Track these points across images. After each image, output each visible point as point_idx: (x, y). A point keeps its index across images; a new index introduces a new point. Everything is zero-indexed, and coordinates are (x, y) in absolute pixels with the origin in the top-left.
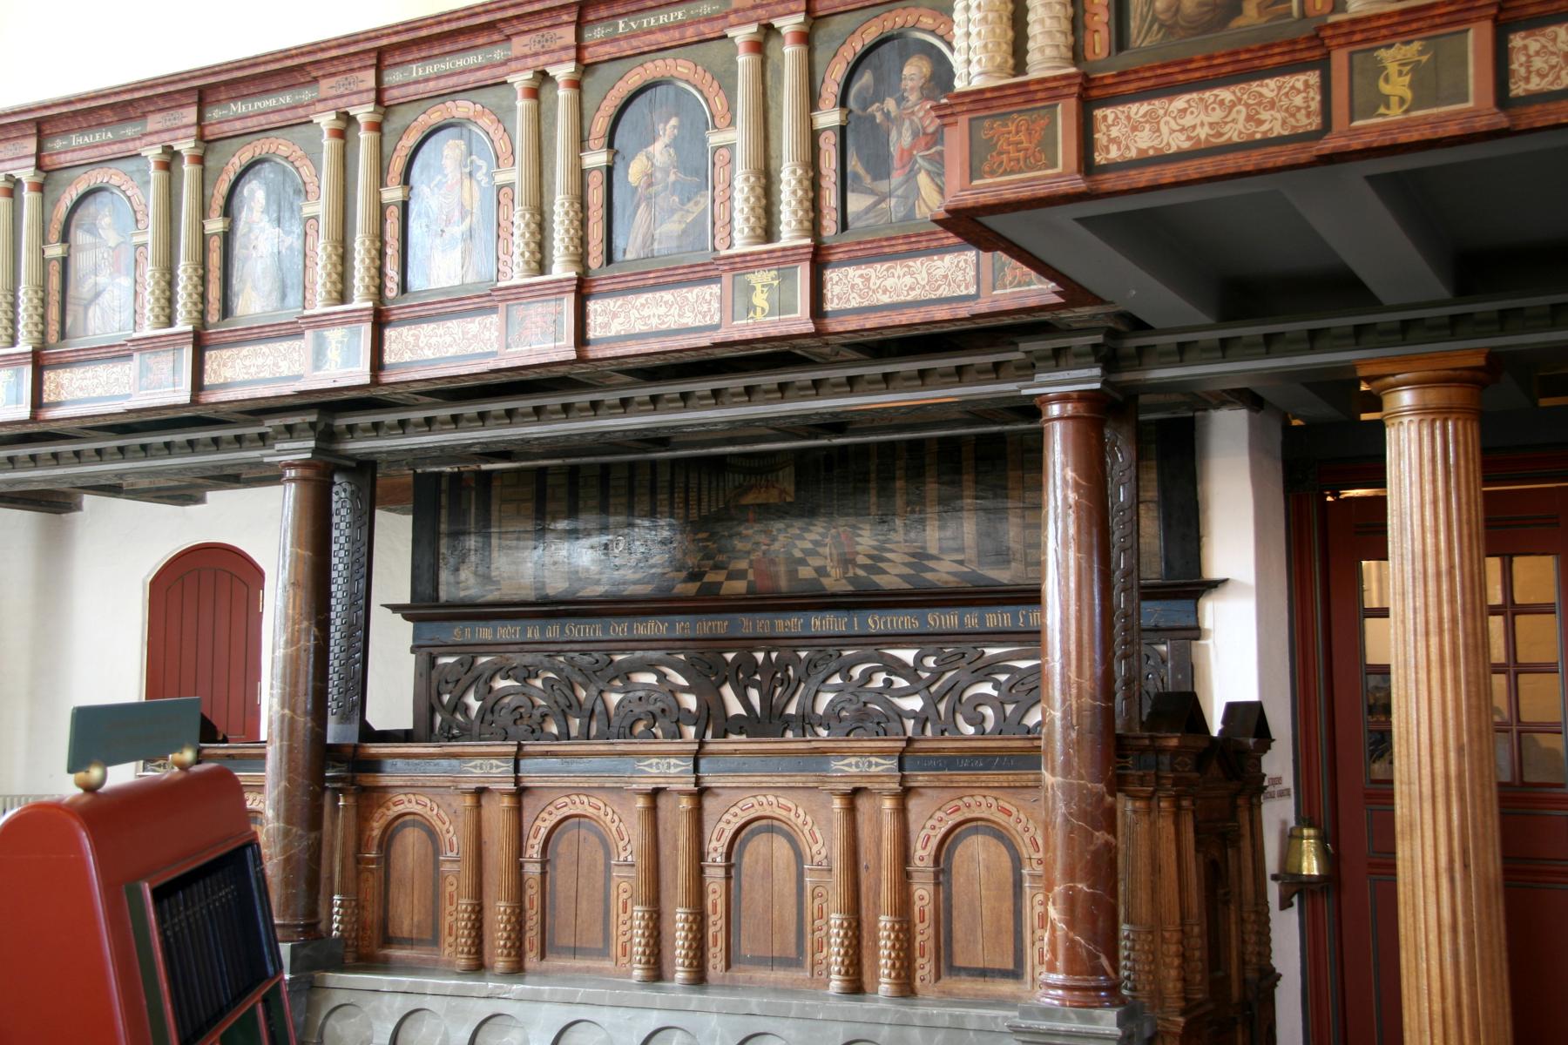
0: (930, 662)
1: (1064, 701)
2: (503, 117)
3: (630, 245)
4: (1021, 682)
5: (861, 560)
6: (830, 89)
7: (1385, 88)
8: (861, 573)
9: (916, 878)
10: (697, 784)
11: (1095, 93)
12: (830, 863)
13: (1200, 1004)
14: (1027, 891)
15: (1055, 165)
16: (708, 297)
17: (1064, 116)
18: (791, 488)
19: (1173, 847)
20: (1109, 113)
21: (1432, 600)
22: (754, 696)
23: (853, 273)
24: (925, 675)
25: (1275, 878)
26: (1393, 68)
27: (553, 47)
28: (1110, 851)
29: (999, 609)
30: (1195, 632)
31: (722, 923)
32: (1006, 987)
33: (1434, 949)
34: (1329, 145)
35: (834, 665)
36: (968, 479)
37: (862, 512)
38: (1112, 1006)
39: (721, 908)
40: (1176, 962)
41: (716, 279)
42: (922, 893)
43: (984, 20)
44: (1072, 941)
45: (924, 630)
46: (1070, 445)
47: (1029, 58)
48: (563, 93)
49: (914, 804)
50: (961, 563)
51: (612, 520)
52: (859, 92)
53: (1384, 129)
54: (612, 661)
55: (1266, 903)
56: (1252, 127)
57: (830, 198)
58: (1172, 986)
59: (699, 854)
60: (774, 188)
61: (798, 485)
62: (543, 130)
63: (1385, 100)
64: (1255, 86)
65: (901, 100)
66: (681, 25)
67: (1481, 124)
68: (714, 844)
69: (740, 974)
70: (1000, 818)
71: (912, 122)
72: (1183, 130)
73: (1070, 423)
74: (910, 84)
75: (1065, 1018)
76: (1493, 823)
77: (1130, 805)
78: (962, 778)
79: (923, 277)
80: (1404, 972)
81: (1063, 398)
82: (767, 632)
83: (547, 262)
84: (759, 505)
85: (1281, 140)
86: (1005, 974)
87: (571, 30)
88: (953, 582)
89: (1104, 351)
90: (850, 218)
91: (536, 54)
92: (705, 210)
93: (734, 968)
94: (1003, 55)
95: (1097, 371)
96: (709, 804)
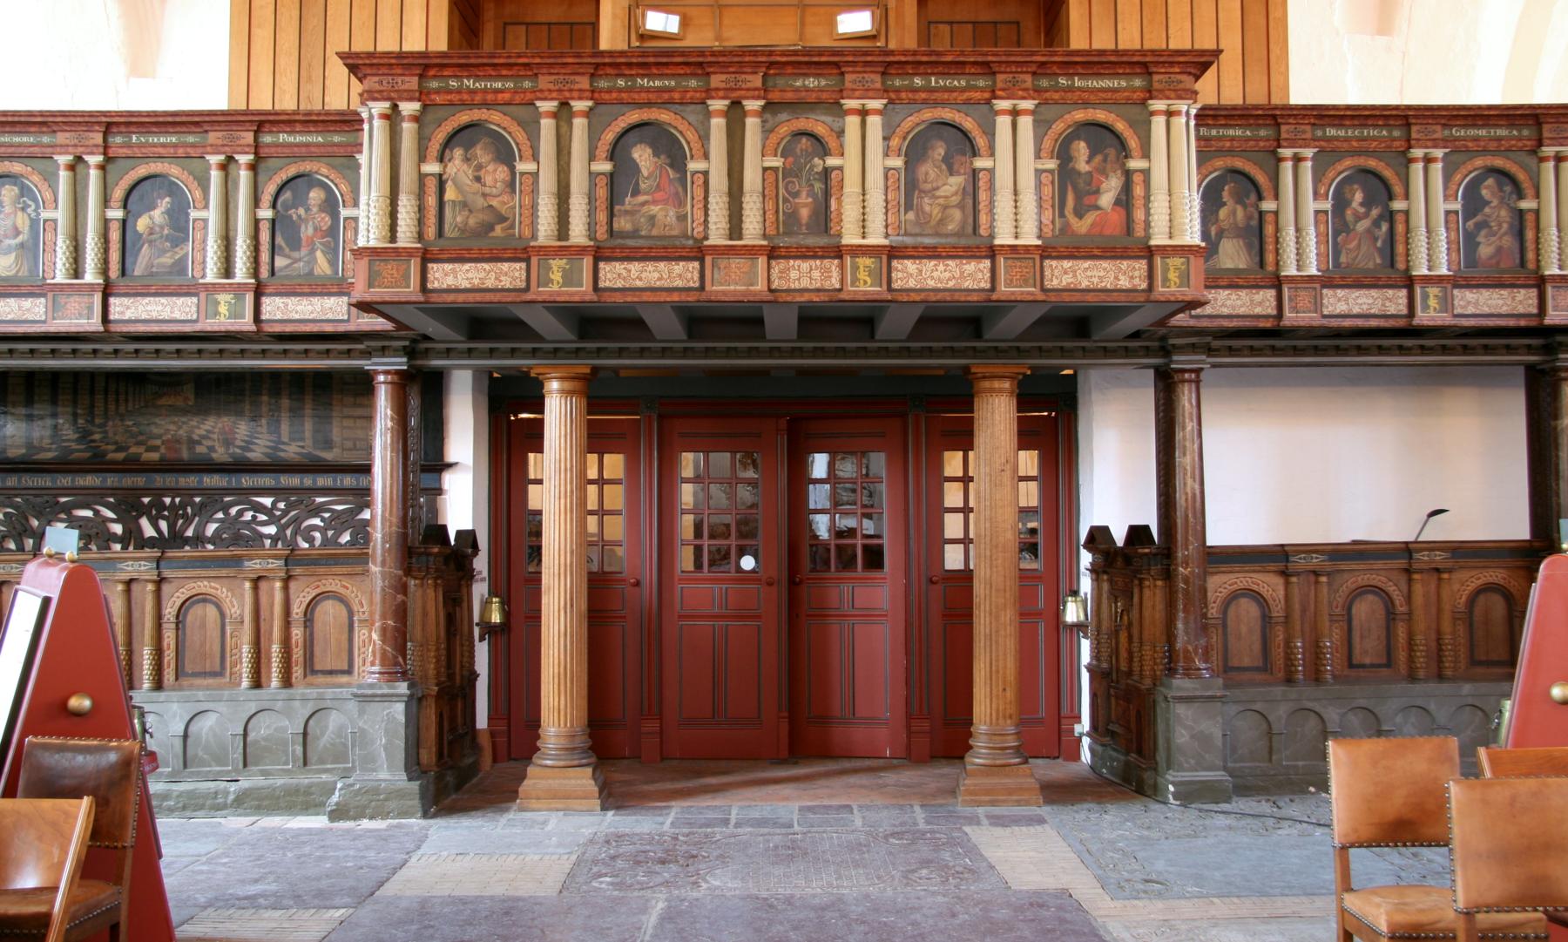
0: (282, 505)
1: (383, 529)
2: (51, 179)
3: (139, 268)
4: (338, 518)
5: (238, 443)
6: (266, 198)
7: (552, 276)
8: (238, 451)
9: (293, 625)
10: (158, 576)
11: (428, 256)
12: (242, 618)
13: (444, 682)
14: (356, 629)
15: (409, 287)
17: (414, 265)
18: (192, 397)
19: (434, 603)
21: (562, 482)
22: (163, 525)
23: (279, 301)
24: (278, 513)
25: (477, 624)
26: (555, 269)
27: (87, 143)
28: (404, 603)
29: (326, 475)
30: (439, 491)
31: (173, 655)
32: (344, 679)
33: (556, 645)
34: (529, 297)
35: (218, 506)
36: (308, 398)
37: (240, 414)
38: (404, 681)
39: (173, 646)
40: (434, 660)
41: (196, 295)
42: (297, 633)
43: (377, 214)
44: (385, 650)
45: (278, 486)
46: (389, 397)
47: (398, 235)
48: (94, 174)
49: (293, 585)
50: (303, 447)
51: (60, 409)
52: (284, 201)
53: (551, 294)
54: (58, 502)
55: (473, 637)
57: (265, 257)
58: (432, 672)
59: (159, 616)
60: (232, 247)
61: (197, 394)
62: (78, 190)
63: (552, 281)
65: (308, 210)
66: (175, 146)
68: (168, 610)
69: (185, 682)
70: (342, 591)
73: (389, 386)
74: (313, 202)
75: (380, 688)
76: (585, 586)
77: (413, 582)
78: (322, 570)
79: (318, 308)
80: (543, 656)
81: (386, 373)
82: (173, 485)
83: (80, 270)
84: (170, 406)
85: (508, 290)
86: (343, 672)
87: (101, 135)
88: (297, 458)
89: (408, 350)
90: (276, 269)
91: (75, 146)
92: (187, 254)
93: (180, 679)
94: (386, 232)
95: (405, 360)
96: (166, 588)
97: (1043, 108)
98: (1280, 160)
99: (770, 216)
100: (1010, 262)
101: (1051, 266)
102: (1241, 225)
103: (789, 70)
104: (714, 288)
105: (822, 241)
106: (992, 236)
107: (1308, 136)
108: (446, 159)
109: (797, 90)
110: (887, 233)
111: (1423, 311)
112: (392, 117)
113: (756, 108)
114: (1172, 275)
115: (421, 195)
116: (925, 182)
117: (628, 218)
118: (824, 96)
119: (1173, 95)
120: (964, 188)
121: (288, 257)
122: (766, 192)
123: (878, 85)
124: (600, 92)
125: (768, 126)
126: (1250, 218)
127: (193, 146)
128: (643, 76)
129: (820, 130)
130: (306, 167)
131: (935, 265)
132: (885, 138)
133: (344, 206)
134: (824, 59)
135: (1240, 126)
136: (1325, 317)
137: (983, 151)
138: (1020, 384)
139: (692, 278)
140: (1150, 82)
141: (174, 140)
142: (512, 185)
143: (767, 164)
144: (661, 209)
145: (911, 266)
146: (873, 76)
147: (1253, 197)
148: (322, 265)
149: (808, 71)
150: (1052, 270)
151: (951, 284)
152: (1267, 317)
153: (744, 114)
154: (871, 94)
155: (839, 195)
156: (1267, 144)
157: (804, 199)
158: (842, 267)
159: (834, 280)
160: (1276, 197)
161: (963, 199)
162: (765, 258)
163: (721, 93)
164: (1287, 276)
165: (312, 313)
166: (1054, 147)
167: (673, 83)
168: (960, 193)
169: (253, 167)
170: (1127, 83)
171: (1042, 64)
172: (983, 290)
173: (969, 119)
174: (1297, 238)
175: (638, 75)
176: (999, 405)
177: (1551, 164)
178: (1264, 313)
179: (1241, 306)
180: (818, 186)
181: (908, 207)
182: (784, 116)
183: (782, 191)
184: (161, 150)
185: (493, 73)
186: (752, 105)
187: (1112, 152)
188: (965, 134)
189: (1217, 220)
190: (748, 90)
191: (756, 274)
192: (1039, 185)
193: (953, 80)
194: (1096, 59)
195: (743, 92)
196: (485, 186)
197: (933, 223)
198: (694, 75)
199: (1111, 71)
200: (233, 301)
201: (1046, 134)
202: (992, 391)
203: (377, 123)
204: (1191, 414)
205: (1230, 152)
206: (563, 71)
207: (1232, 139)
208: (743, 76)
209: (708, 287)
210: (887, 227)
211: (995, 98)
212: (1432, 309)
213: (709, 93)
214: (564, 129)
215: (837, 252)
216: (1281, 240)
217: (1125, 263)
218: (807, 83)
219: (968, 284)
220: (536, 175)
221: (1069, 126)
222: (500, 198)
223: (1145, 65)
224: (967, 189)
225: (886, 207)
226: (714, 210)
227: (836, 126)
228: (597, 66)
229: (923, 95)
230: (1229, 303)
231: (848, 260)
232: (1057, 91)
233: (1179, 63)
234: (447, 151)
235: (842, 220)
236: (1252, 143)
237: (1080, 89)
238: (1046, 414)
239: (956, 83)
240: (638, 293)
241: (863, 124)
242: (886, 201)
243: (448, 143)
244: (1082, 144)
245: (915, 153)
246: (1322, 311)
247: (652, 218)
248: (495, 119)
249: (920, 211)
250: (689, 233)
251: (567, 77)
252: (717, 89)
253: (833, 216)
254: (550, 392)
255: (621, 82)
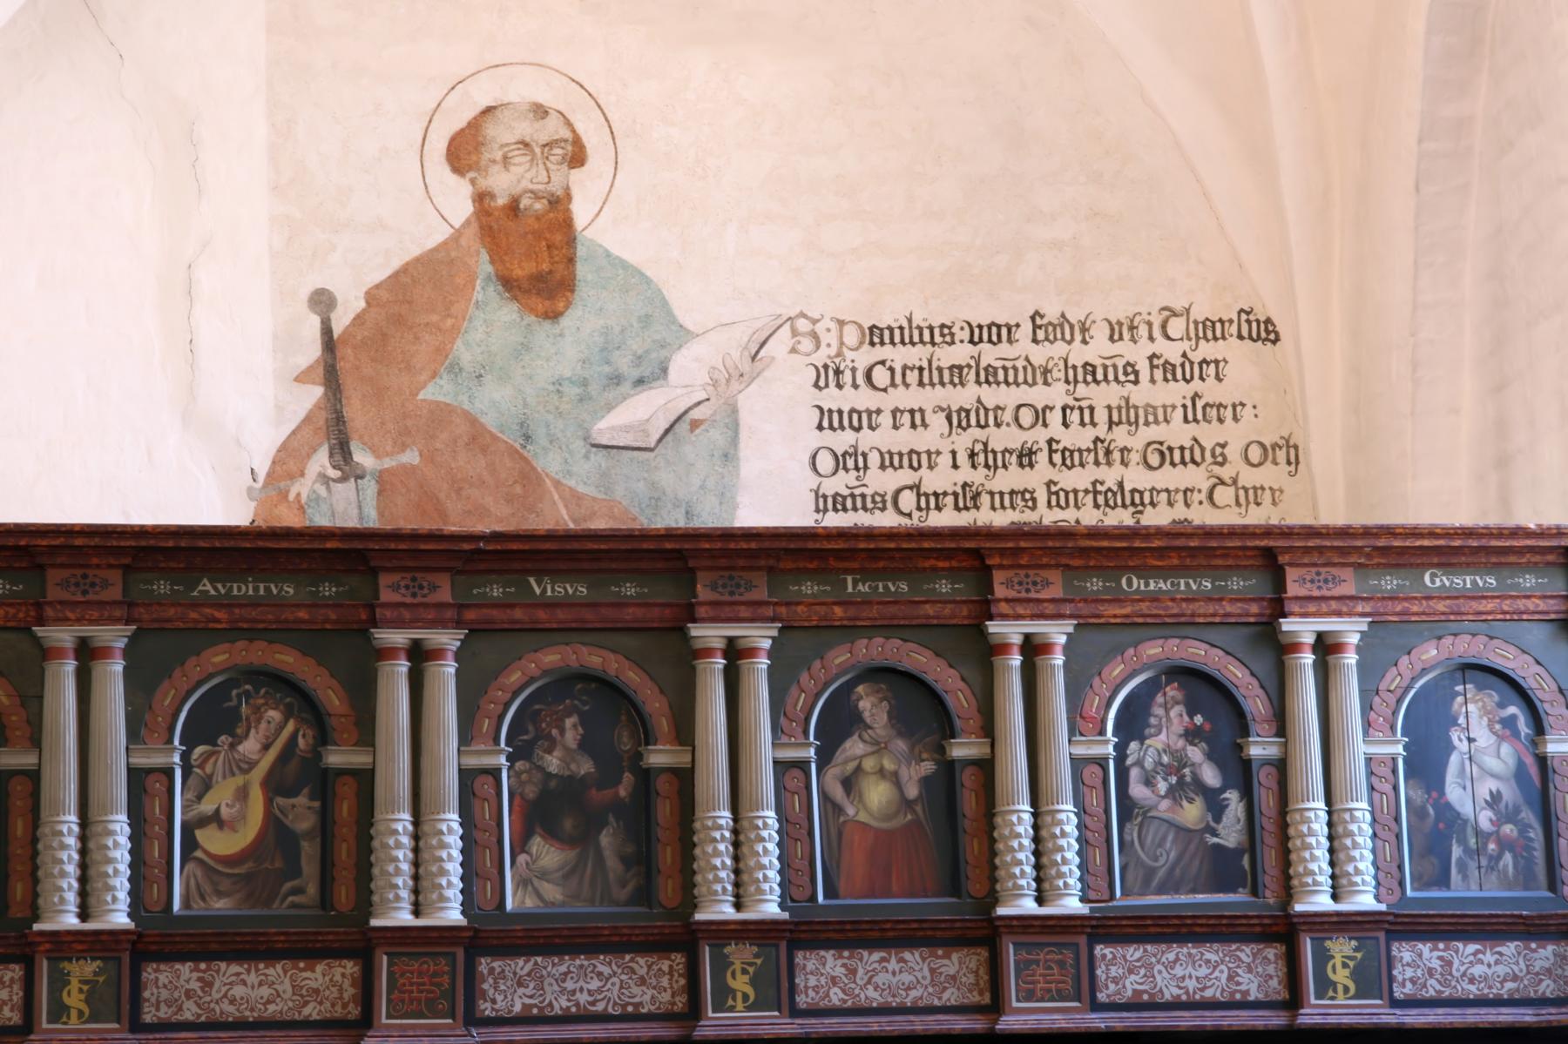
98: (47, 654)
111: (1319, 996)
131: (883, 960)
177: (402, 666)
212: (74, 1014)
246: (1391, 991)
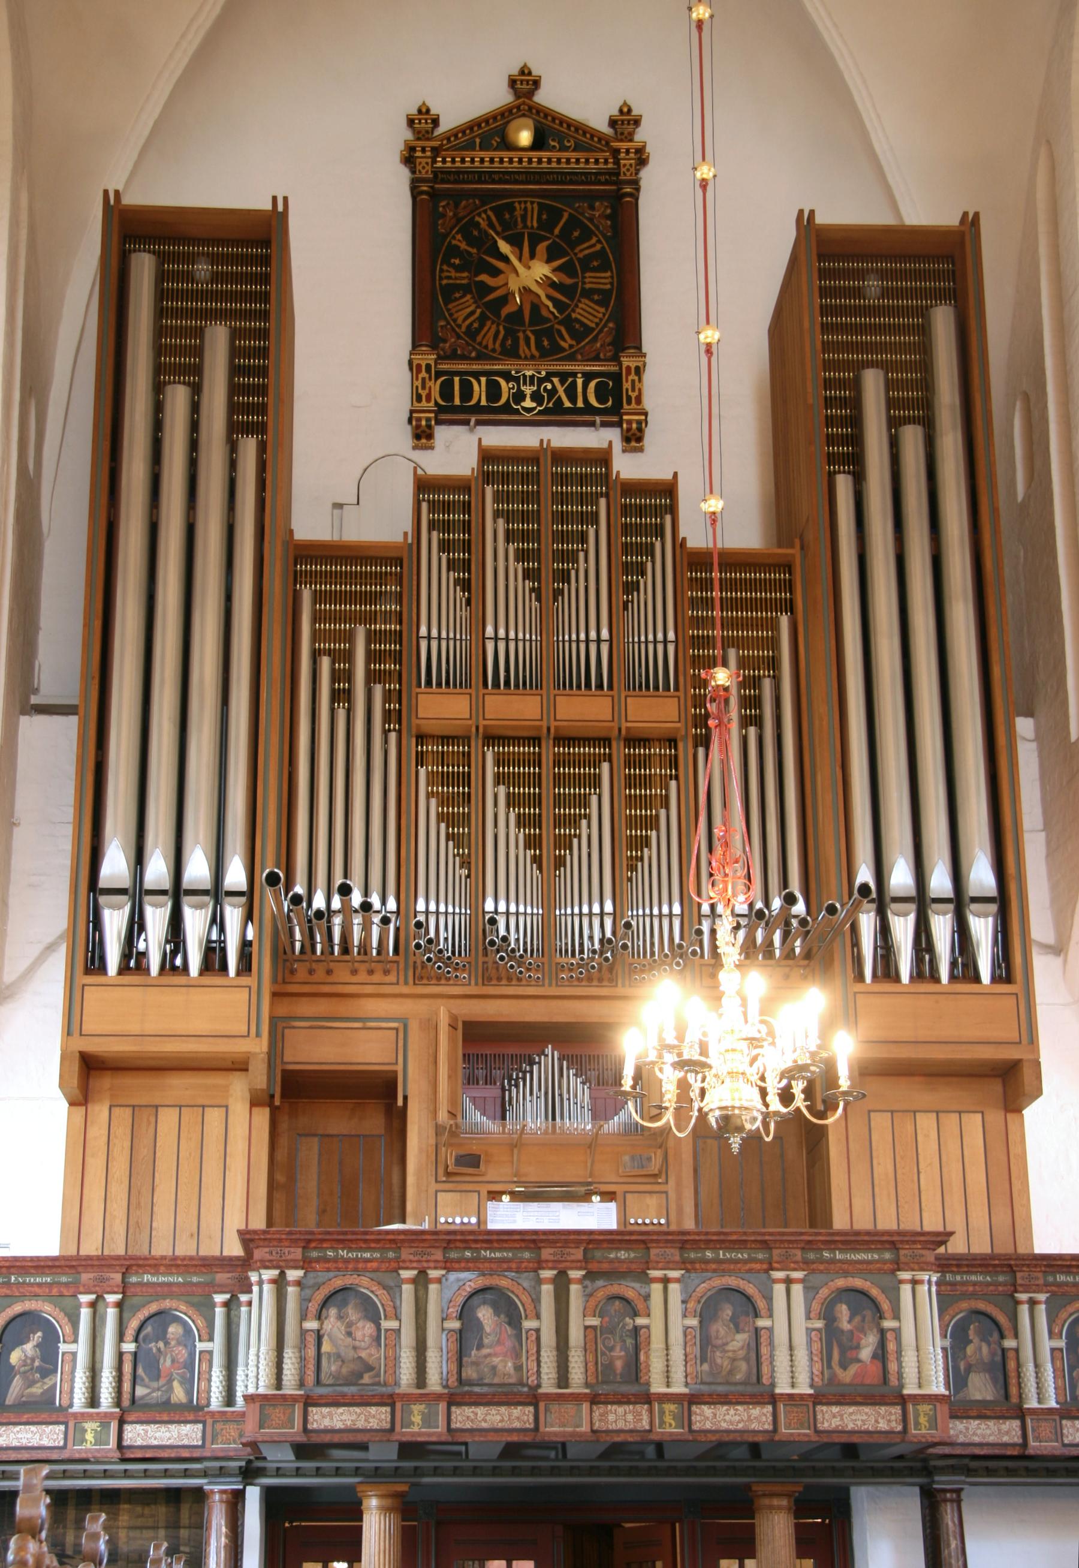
6: (130, 1333)
7: (413, 1419)
15: (294, 1428)
16: (57, 1431)
20: (314, 1409)
23: (139, 1428)
26: (416, 1412)
47: (284, 1383)
53: (413, 1434)
56: (366, 1424)
57: (127, 1386)
60: (97, 1378)
63: (413, 1423)
64: (368, 1408)
65: (166, 1343)
67: (443, 1439)
71: (172, 1355)
72: (341, 1421)
74: (172, 1336)
90: (136, 1398)
92: (55, 1384)
97: (811, 1278)
98: (1017, 1303)
99: (591, 1366)
100: (788, 1408)
101: (822, 1411)
102: (986, 1361)
103: (605, 1245)
104: (547, 1429)
105: (633, 1389)
106: (773, 1385)
107: (1041, 1282)
108: (323, 1317)
109: (611, 1261)
110: (686, 1382)
112: (280, 1283)
113: (578, 1276)
114: (923, 1420)
115: (302, 1345)
116: (717, 1338)
117: (474, 1368)
118: (634, 1266)
119: (916, 1267)
120: (749, 1344)
121: (147, 1387)
122: (587, 1347)
123: (677, 1258)
124: (452, 1262)
125: (588, 1291)
126: (993, 1354)
127: (67, 1284)
128: (485, 1249)
129: (630, 1294)
130: (167, 1304)
131: (727, 1410)
132: (683, 1302)
133: (200, 1340)
134: (633, 1238)
135: (981, 1273)
136: (1064, 1445)
137: (763, 1312)
138: (797, 1501)
139: (528, 1420)
140: (898, 1256)
141: (49, 1280)
142: (378, 1339)
143: (588, 1323)
144: (501, 1361)
145: (707, 1410)
146: (672, 1250)
147: (996, 1335)
148: (179, 1394)
149: (620, 1246)
150: (823, 1414)
151: (740, 1426)
152: (1014, 1445)
153: (569, 1281)
154: (671, 1265)
155: (647, 1350)
156: (1005, 1288)
157: (618, 1353)
158: (651, 1411)
159: (644, 1423)
160: (1016, 1336)
161: (748, 1353)
162: (588, 1404)
163: (550, 1265)
164: (1029, 1409)
165: (169, 1439)
166: (821, 1309)
167: (510, 1255)
168: (746, 1347)
169: (119, 1305)
170: (879, 1255)
171: (809, 1242)
172: (766, 1431)
173: (751, 1285)
174: (1037, 1373)
175: (482, 1248)
176: (779, 1522)
178: (1011, 1441)
179: (990, 1435)
180: (630, 1342)
181: (703, 1360)
182: (600, 1283)
183: (600, 1346)
184: (37, 1290)
185: (364, 1246)
186: (575, 1274)
187: (868, 1313)
188: (748, 1298)
189: (965, 1356)
190: (573, 1261)
191: (581, 1418)
192: (810, 1342)
193: (738, 1253)
194: (853, 1238)
195: (568, 1264)
196: (355, 1340)
197: (724, 1373)
198: (527, 1248)
199: (865, 1247)
200: (99, 1429)
201: (814, 1298)
202: (771, 1508)
203: (266, 1287)
204: (954, 1532)
205: (973, 1296)
206: (422, 1245)
207: (975, 1284)
208: (568, 1250)
209: (542, 1429)
210: (686, 1377)
211: (772, 1270)
213: (540, 1265)
214: (421, 1293)
215: (647, 1398)
216: (1022, 1375)
217: (883, 1408)
218: (619, 1255)
219: (754, 1426)
220: (398, 1331)
221: (833, 1292)
222: (368, 1351)
223: (893, 1243)
224: (751, 1344)
225: (686, 1361)
226: (546, 1363)
227: (643, 1292)
228: (449, 1241)
229: (714, 1266)
230: (979, 1432)
231: (656, 1406)
232: (822, 1263)
233: (920, 1241)
234: (324, 1311)
235: (649, 1371)
236: (991, 1288)
237: (840, 1261)
238: (819, 1520)
239: (740, 1255)
240: (483, 1433)
241: (665, 1290)
242: (686, 1355)
243: (325, 1303)
244: (844, 1307)
245: (707, 1313)
247: (494, 1368)
248: (365, 1284)
249: (713, 1363)
250: (525, 1380)
251: (424, 1250)
252: (547, 1261)
253: (643, 1366)
254: (369, 1509)
255: (468, 1254)
